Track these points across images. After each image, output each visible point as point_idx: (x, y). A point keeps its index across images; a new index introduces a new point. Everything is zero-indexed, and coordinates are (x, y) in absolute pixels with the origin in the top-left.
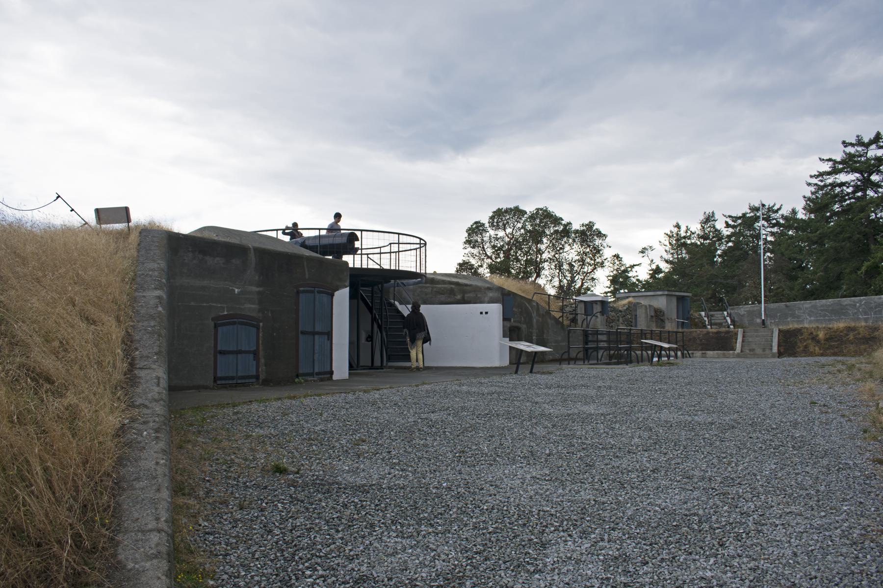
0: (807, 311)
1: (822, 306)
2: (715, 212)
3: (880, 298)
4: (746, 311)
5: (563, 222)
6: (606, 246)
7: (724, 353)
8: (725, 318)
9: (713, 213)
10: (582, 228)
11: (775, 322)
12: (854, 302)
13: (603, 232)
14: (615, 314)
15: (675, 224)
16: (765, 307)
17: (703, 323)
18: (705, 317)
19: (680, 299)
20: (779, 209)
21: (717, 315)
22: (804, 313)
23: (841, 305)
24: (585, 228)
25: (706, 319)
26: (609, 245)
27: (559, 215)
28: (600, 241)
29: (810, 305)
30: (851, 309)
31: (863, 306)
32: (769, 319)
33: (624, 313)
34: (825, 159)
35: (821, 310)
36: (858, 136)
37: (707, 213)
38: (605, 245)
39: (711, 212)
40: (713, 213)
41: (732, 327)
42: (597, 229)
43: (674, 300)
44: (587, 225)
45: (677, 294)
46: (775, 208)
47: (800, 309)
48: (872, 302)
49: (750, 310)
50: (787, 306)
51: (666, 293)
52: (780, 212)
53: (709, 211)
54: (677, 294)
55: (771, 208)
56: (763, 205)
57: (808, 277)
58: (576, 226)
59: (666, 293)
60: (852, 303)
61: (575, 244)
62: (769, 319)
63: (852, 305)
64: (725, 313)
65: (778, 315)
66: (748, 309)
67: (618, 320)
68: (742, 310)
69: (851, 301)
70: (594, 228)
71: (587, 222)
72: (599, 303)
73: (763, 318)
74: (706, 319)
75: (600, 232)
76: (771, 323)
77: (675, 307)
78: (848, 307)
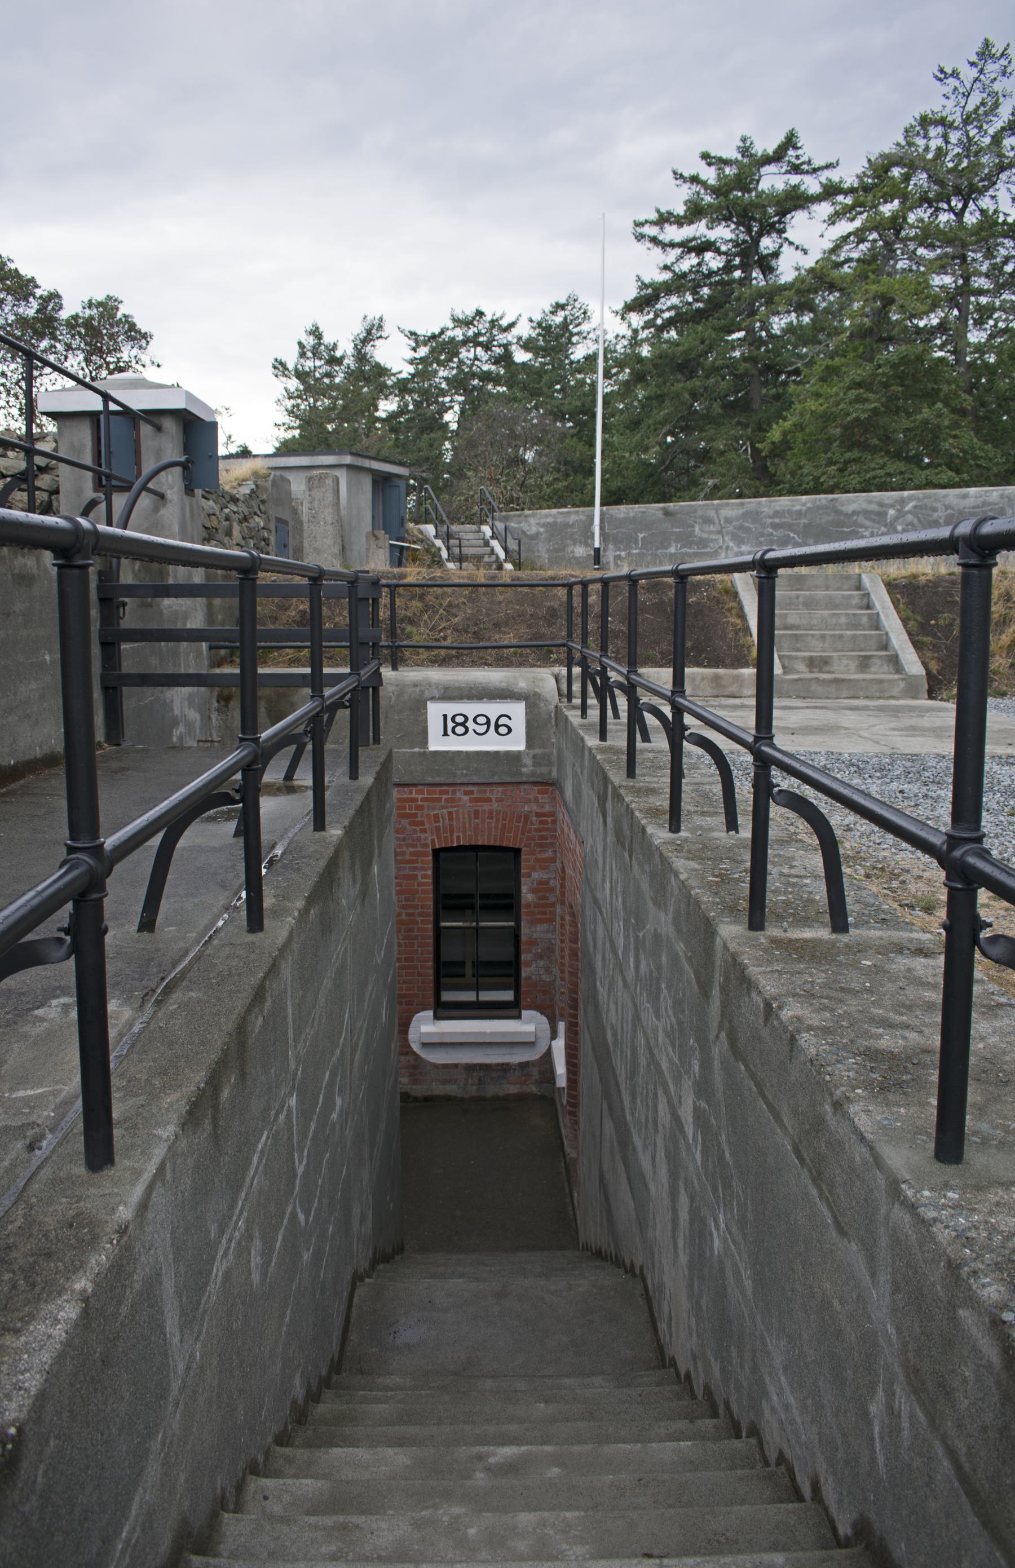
0: (730, 528)
1: (776, 514)
2: (384, 318)
3: (965, 496)
4: (543, 525)
5: (38, 292)
6: (148, 363)
7: (717, 678)
8: (487, 544)
9: (381, 319)
10: (88, 312)
11: (629, 554)
12: (881, 504)
13: (142, 326)
14: (217, 509)
15: (309, 327)
16: (602, 514)
17: (434, 556)
18: (436, 537)
19: (382, 482)
20: (512, 325)
21: (464, 531)
22: (720, 532)
23: (838, 512)
24: (94, 312)
25: (439, 543)
26: (157, 361)
27: (26, 272)
28: (135, 352)
29: (741, 511)
30: (868, 523)
31: (910, 517)
32: (611, 546)
33: (242, 508)
34: (686, 174)
35: (776, 526)
36: (744, 140)
37: (370, 318)
38: (145, 358)
39: (377, 317)
40: (381, 319)
41: (509, 566)
42: (125, 316)
43: (367, 483)
44: (100, 304)
45: (376, 465)
46: (504, 323)
47: (708, 521)
48: (939, 505)
49: (555, 523)
50: (667, 513)
51: (348, 459)
52: (515, 331)
53: (373, 314)
54: (376, 465)
55: (497, 320)
56: (480, 314)
57: (624, 457)
58: (70, 308)
59: (348, 459)
60: (874, 507)
61: (70, 356)
62: (611, 546)
63: (872, 512)
64: (486, 530)
65: (641, 536)
66: (550, 520)
67: (229, 533)
68: (532, 521)
69: (870, 502)
70: (119, 315)
71: (100, 297)
72: (170, 425)
73: (597, 545)
74: (439, 543)
75: (132, 327)
76: (618, 558)
77: (370, 504)
78: (861, 519)
